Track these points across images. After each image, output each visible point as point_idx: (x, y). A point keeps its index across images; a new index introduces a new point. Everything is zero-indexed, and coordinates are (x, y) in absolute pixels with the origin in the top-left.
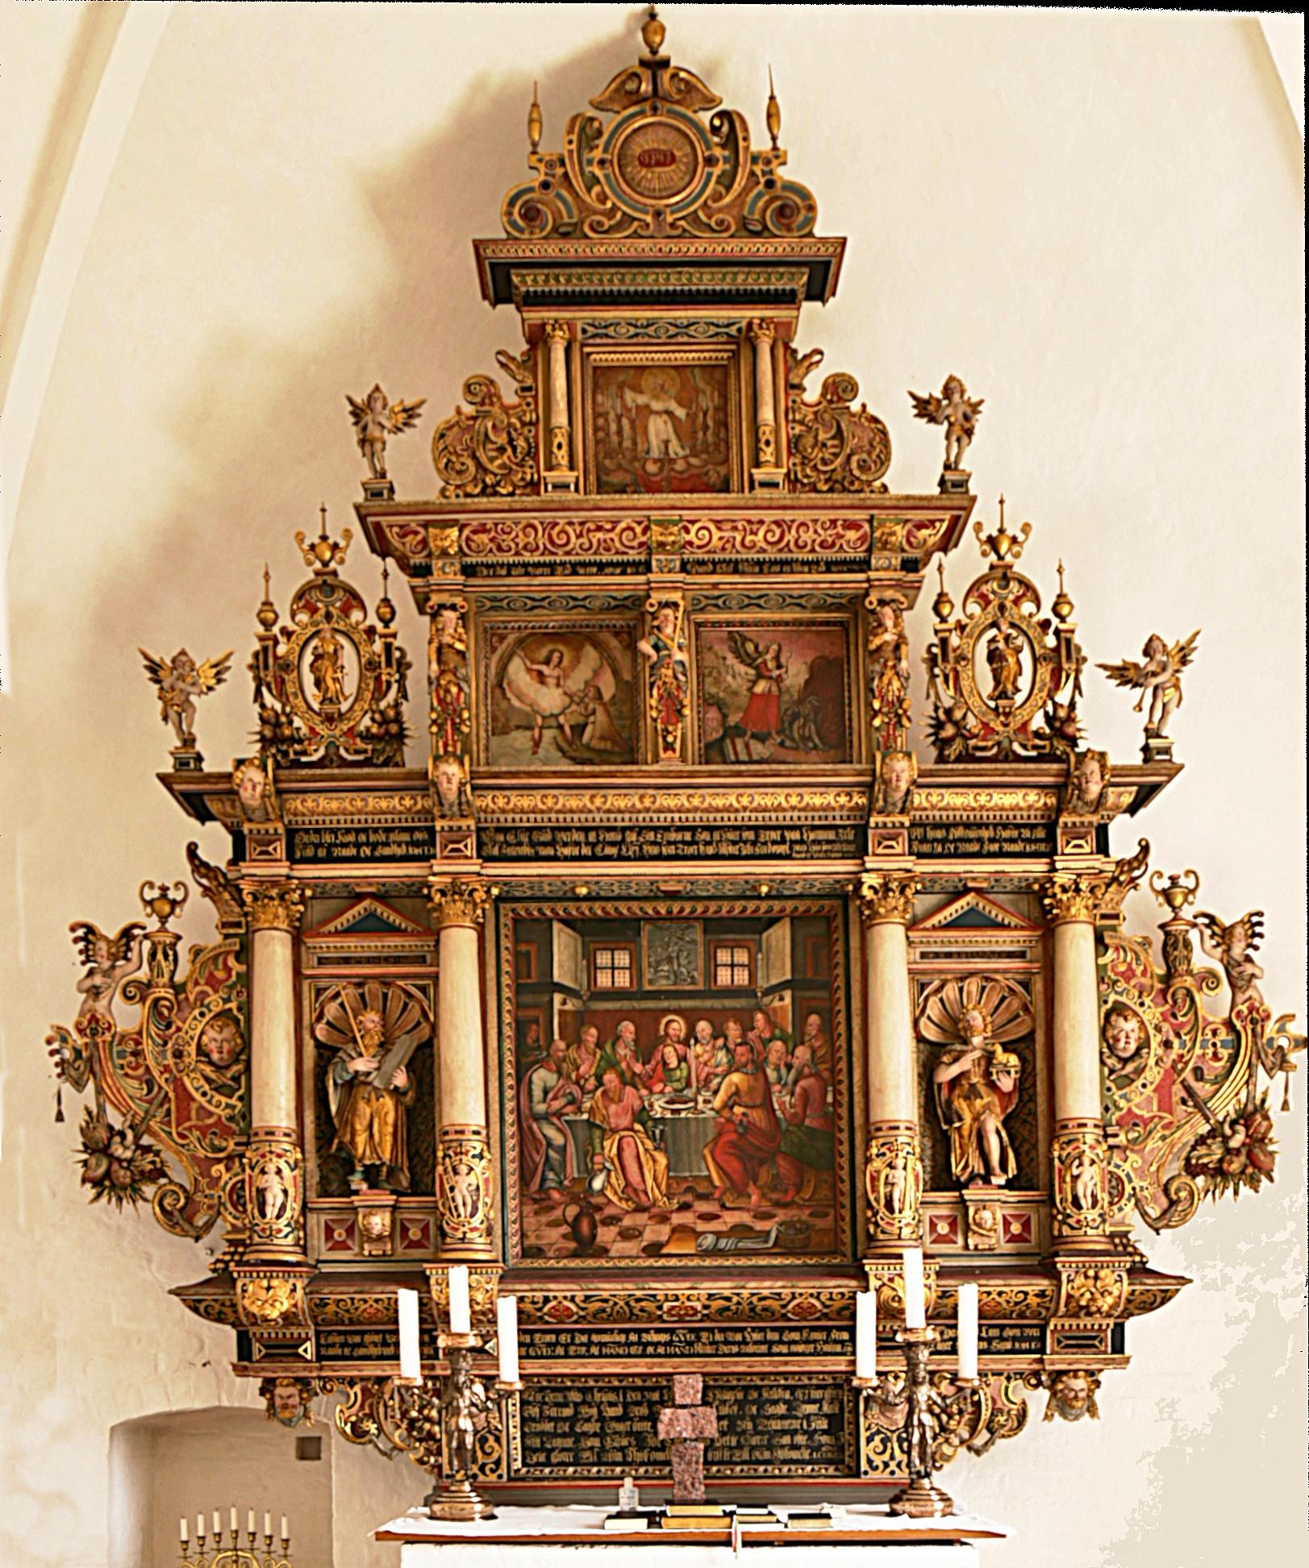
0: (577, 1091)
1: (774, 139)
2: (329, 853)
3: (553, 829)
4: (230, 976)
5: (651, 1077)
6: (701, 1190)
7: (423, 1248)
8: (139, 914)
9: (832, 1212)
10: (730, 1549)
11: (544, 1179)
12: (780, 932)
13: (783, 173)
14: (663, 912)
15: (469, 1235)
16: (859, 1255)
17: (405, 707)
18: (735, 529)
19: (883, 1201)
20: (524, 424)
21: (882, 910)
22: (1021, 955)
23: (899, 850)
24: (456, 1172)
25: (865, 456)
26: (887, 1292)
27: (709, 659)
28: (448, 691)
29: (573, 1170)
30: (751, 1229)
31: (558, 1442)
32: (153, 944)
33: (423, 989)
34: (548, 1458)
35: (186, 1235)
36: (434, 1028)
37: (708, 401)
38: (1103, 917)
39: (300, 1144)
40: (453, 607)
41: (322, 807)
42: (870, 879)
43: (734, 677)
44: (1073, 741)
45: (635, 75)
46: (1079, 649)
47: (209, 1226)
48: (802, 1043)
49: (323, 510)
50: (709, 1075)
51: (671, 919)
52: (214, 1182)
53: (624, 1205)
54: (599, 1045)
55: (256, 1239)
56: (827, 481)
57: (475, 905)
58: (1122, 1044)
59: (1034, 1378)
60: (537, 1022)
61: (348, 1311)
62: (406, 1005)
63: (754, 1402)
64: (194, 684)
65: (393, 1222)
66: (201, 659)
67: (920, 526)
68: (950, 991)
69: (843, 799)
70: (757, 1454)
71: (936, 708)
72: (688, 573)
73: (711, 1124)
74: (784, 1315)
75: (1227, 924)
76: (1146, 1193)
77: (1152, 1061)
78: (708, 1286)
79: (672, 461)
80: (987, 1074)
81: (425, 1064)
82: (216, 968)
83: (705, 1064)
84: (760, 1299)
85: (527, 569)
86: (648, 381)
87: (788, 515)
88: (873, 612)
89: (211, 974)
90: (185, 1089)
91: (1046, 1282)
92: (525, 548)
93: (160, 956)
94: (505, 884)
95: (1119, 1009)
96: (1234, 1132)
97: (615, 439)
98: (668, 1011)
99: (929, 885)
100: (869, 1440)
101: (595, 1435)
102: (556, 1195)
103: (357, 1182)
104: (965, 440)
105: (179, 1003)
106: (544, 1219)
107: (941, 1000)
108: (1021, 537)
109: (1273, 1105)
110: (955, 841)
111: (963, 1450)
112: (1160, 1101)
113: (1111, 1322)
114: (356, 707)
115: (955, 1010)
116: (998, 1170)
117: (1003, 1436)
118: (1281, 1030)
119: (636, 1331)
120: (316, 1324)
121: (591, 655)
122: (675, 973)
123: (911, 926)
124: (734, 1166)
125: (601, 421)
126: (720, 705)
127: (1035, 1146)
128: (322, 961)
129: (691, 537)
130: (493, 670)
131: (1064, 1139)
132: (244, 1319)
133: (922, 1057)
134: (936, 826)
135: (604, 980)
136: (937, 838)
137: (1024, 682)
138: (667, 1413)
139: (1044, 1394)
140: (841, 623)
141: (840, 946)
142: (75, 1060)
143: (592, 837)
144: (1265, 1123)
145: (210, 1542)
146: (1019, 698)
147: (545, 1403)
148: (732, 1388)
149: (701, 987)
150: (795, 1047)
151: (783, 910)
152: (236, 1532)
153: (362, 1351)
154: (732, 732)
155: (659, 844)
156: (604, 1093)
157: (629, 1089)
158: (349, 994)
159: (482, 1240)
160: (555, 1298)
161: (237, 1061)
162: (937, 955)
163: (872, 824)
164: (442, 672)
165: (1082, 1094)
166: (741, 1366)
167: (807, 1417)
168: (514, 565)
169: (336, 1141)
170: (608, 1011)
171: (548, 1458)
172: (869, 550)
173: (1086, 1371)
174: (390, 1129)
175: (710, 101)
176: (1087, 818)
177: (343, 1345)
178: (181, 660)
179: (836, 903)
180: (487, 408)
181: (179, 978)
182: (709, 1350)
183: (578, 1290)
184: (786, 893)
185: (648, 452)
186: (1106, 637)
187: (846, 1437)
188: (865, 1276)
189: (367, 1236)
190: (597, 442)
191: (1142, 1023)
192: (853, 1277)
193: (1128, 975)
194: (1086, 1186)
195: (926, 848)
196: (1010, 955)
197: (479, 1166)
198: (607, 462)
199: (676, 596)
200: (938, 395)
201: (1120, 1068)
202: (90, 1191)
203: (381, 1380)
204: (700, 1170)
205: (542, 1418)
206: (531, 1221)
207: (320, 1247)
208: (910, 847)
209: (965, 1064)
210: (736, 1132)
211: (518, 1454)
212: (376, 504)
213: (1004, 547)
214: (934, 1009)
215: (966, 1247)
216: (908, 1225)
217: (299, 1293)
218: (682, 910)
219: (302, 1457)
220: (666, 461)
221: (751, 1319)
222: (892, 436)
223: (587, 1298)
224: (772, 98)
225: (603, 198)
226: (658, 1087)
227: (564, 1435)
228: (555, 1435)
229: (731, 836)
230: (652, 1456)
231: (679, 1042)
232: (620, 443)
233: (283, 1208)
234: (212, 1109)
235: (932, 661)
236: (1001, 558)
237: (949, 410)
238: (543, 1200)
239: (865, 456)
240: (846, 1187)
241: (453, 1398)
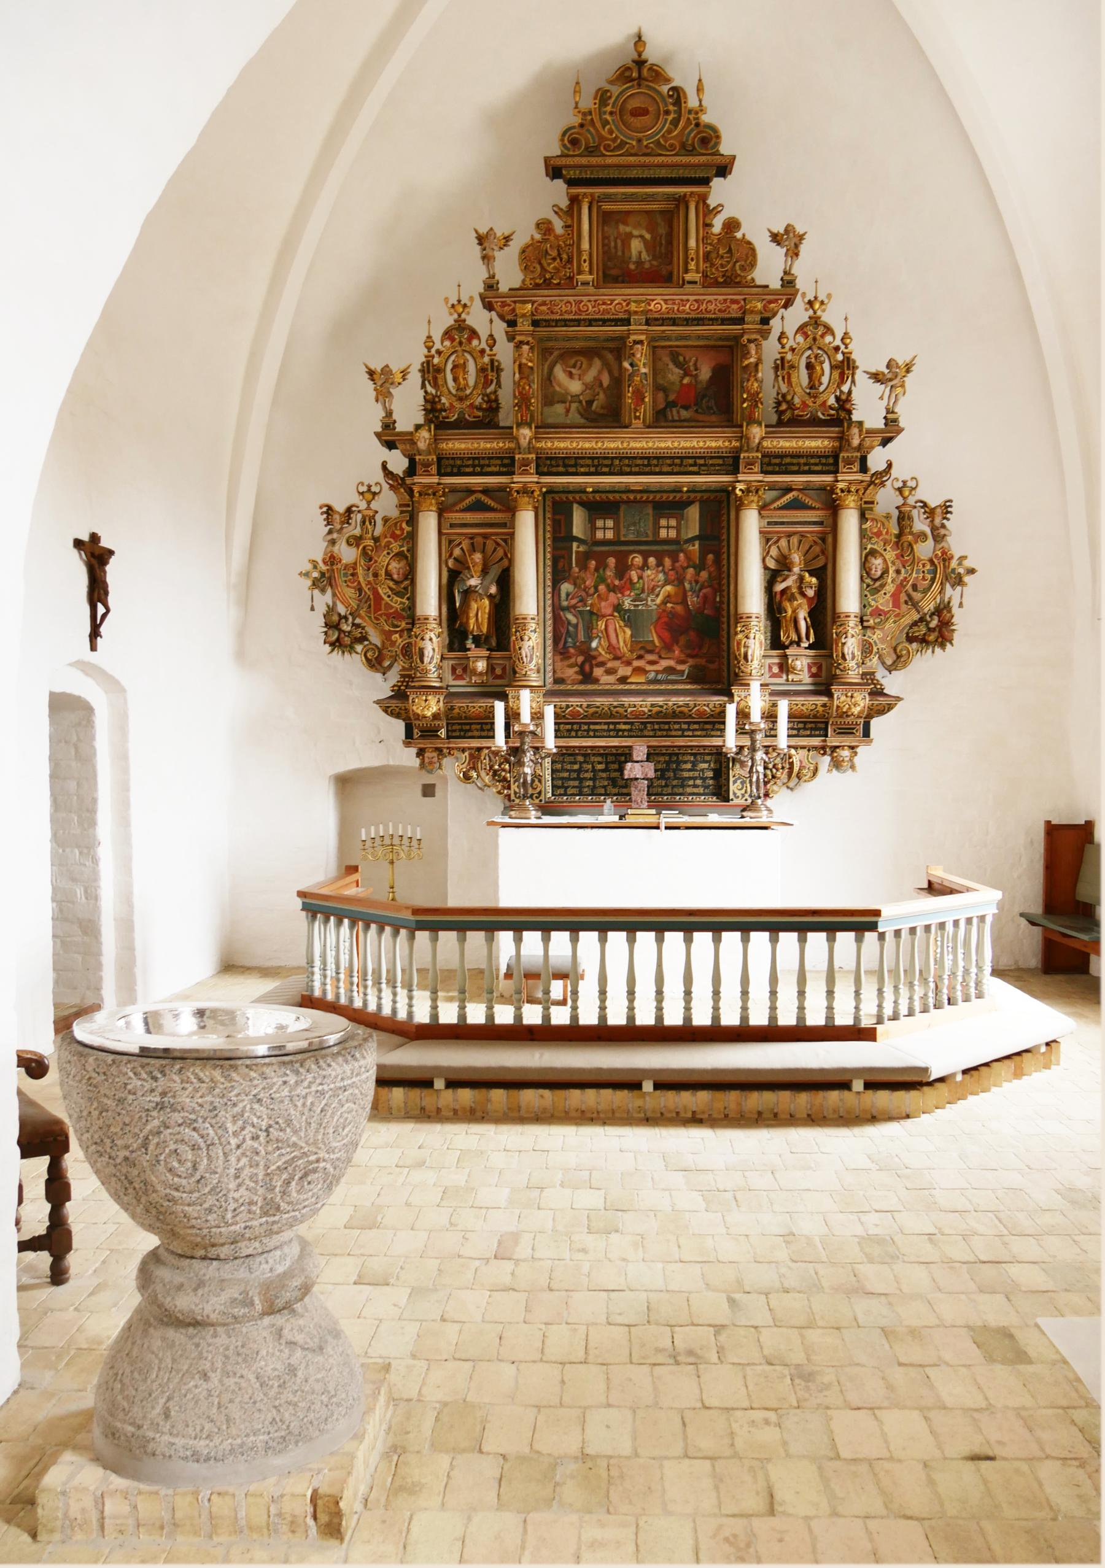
0: (583, 594)
1: (700, 101)
2: (459, 470)
3: (576, 458)
7: (503, 681)
8: (355, 499)
13: (705, 118)
17: (500, 392)
20: (566, 245)
22: (821, 523)
23: (756, 470)
24: (522, 640)
26: (743, 704)
28: (524, 388)
29: (581, 637)
31: (571, 783)
33: (505, 541)
35: (377, 671)
37: (662, 230)
38: (866, 503)
39: (440, 624)
40: (527, 343)
41: (458, 445)
44: (849, 412)
47: (390, 666)
52: (393, 643)
53: (608, 656)
54: (597, 569)
59: (822, 749)
66: (395, 368)
67: (770, 302)
68: (783, 543)
69: (727, 444)
71: (778, 394)
75: (933, 506)
77: (889, 580)
78: (651, 700)
80: (800, 588)
81: (506, 582)
86: (632, 219)
91: (826, 699)
97: (613, 250)
99: (772, 487)
100: (735, 782)
101: (590, 779)
102: (572, 650)
103: (470, 644)
106: (566, 663)
108: (826, 301)
109: (955, 604)
111: (784, 788)
113: (862, 720)
115: (785, 551)
118: (960, 564)
119: (613, 723)
121: (597, 363)
123: (762, 508)
124: (666, 635)
126: (665, 390)
128: (452, 526)
129: (652, 307)
130: (546, 371)
133: (768, 577)
135: (599, 535)
136: (774, 463)
137: (825, 380)
140: (729, 347)
145: (378, 841)
146: (822, 388)
148: (663, 754)
149: (650, 538)
153: (470, 734)
154: (671, 405)
161: (406, 579)
162: (776, 523)
164: (521, 378)
167: (702, 770)
168: (560, 320)
172: (744, 313)
175: (668, 80)
176: (855, 454)
177: (460, 730)
181: (377, 533)
182: (651, 733)
186: (868, 357)
189: (474, 672)
191: (885, 560)
193: (878, 534)
195: (770, 468)
197: (534, 636)
199: (643, 337)
201: (870, 582)
202: (327, 648)
205: (563, 770)
206: (559, 664)
207: (449, 680)
213: (817, 306)
215: (787, 680)
217: (441, 704)
219: (433, 795)
220: (640, 263)
221: (673, 717)
223: (588, 706)
224: (700, 80)
225: (611, 132)
226: (628, 593)
227: (574, 779)
228: (569, 779)
229: (668, 461)
230: (619, 788)
233: (432, 658)
235: (776, 368)
237: (789, 240)
240: (725, 647)
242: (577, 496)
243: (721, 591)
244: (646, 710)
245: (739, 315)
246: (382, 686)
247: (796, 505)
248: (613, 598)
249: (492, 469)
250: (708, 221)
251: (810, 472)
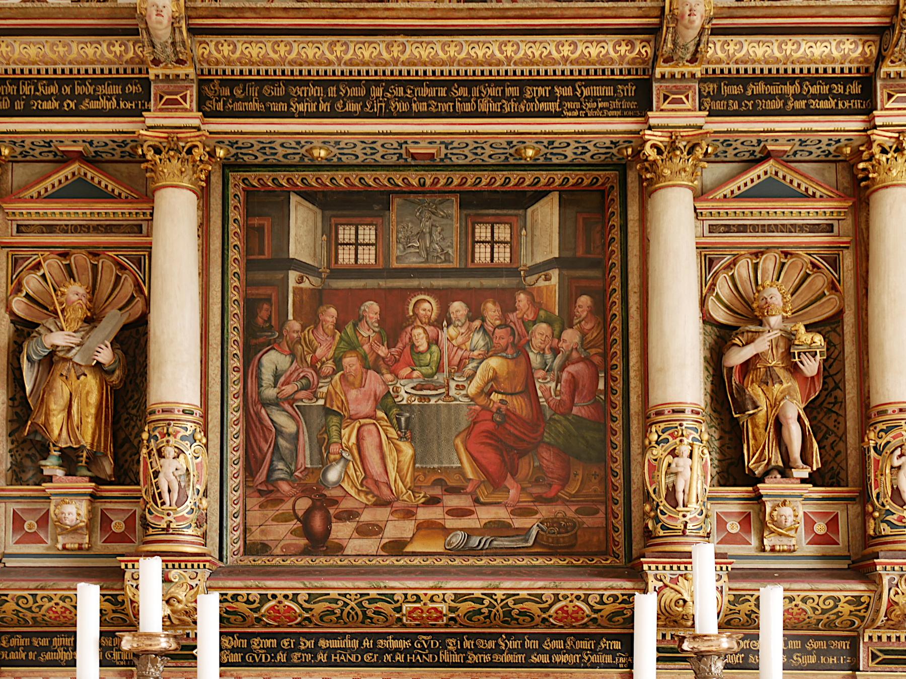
0: (310, 374)
3: (287, 83)
5: (397, 361)
6: (451, 483)
9: (603, 508)
11: (271, 470)
12: (547, 209)
14: (415, 182)
15: (173, 525)
16: (635, 554)
19: (664, 492)
21: (667, 172)
22: (829, 228)
23: (688, 105)
24: (161, 455)
26: (669, 595)
29: (305, 459)
30: (508, 526)
33: (138, 262)
36: (147, 302)
42: (655, 137)
50: (465, 360)
51: (423, 193)
53: (363, 498)
60: (268, 300)
61: (30, 609)
62: (118, 278)
68: (743, 270)
73: (465, 410)
74: (544, 620)
81: (134, 341)
83: (459, 347)
91: (862, 587)
94: (231, 144)
102: (285, 487)
103: (52, 466)
106: (271, 513)
110: (754, 97)
115: (747, 289)
123: (700, 195)
124: (490, 457)
127: (843, 438)
131: (880, 426)
133: (710, 340)
134: (731, 81)
135: (346, 257)
136: (734, 92)
141: (616, 221)
149: (455, 264)
153: (49, 656)
155: (410, 101)
160: (274, 596)
162: (728, 229)
163: (658, 76)
169: (29, 422)
179: (612, 174)
184: (555, 160)
192: (629, 578)
195: (719, 105)
196: (814, 229)
204: (451, 461)
206: (255, 516)
209: (761, 345)
210: (492, 420)
214: (723, 288)
218: (436, 181)
223: (311, 598)
226: (406, 371)
229: (492, 91)
231: (429, 324)
238: (271, 491)
240: (619, 481)
242: (297, 177)
243: (608, 369)
244: (444, 608)
247: (769, 190)
248: (374, 383)
249: (103, 103)
251: (808, 112)
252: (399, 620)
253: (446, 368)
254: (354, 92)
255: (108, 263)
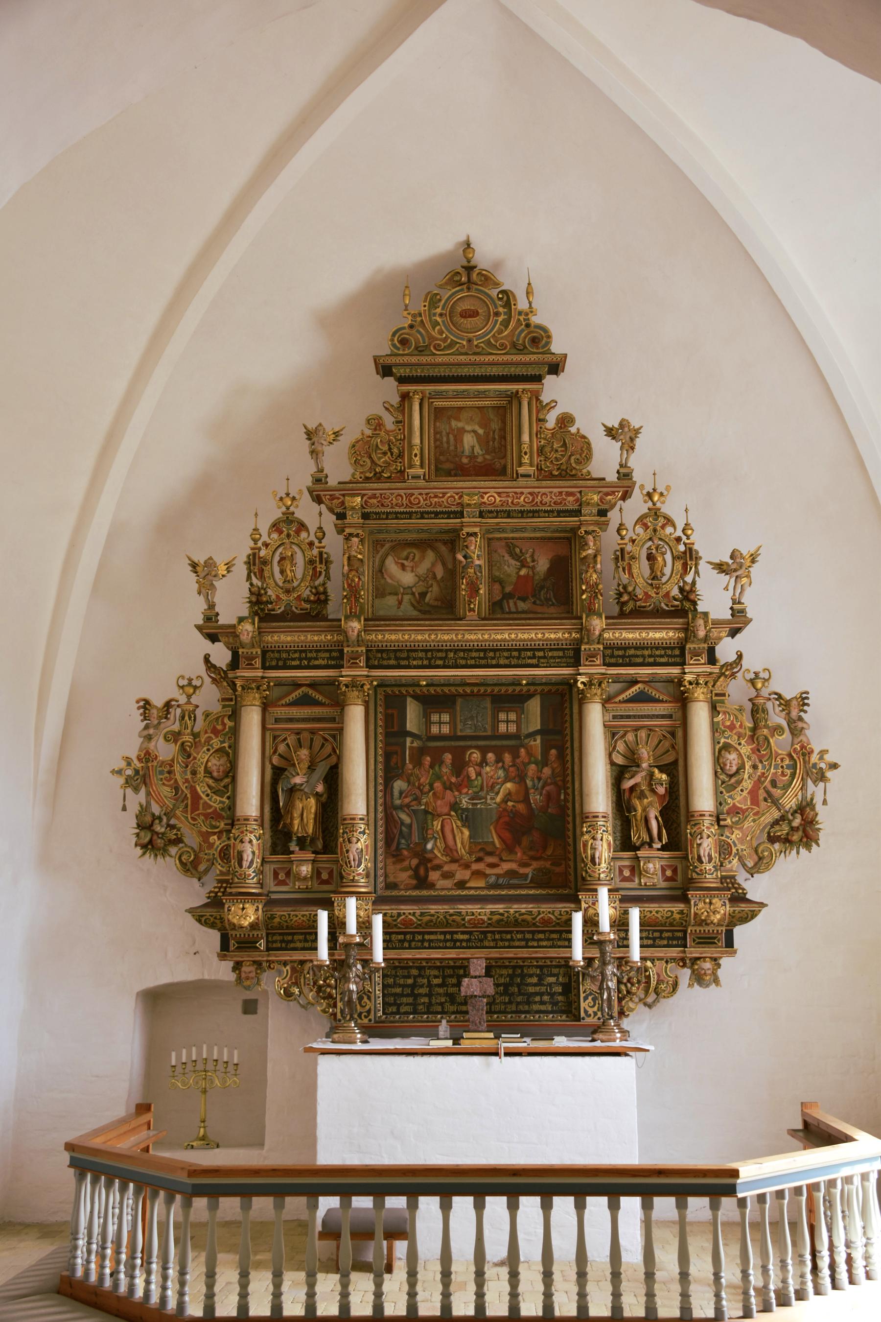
0: (418, 792)
2: (285, 663)
3: (408, 651)
4: (225, 728)
5: (460, 785)
10: (498, 1058)
11: (399, 843)
13: (535, 320)
17: (329, 585)
18: (508, 496)
22: (670, 717)
23: (598, 662)
24: (350, 842)
25: (578, 456)
26: (591, 911)
27: (495, 557)
28: (353, 580)
29: (415, 838)
31: (404, 1000)
32: (182, 710)
33: (334, 737)
34: (398, 1009)
35: (193, 876)
37: (495, 425)
38: (716, 695)
39: (262, 825)
40: (357, 535)
41: (283, 638)
43: (508, 566)
45: (458, 273)
46: (697, 552)
47: (207, 871)
48: (547, 765)
49: (288, 479)
50: (495, 785)
52: (211, 846)
53: (444, 859)
54: (432, 766)
55: (236, 880)
56: (558, 469)
57: (364, 692)
58: (728, 767)
59: (683, 962)
62: (323, 744)
63: (518, 976)
64: (215, 576)
65: (313, 869)
67: (607, 494)
68: (630, 737)
69: (566, 635)
70: (521, 1007)
72: (483, 518)
76: (745, 853)
77: (746, 776)
78: (491, 907)
79: (476, 457)
80: (650, 785)
81: (334, 780)
82: (218, 724)
83: (491, 777)
84: (520, 915)
85: (397, 516)
86: (464, 415)
87: (536, 490)
88: (582, 537)
89: (214, 727)
90: (197, 792)
91: (682, 905)
92: (396, 505)
93: (187, 718)
95: (727, 747)
96: (794, 818)
97: (445, 445)
98: (470, 747)
99: (617, 679)
100: (586, 998)
101: (426, 995)
102: (405, 853)
103: (293, 846)
104: (631, 451)
105: (195, 743)
106: (398, 866)
107: (625, 742)
108: (665, 493)
110: (629, 656)
111: (641, 1006)
112: (751, 799)
113: (724, 929)
114: (302, 584)
115: (632, 745)
116: (657, 840)
117: (664, 997)
119: (450, 933)
120: (267, 929)
122: (475, 725)
124: (507, 835)
125: (438, 436)
126: (501, 582)
128: (277, 721)
129: (485, 500)
131: (693, 823)
132: (227, 926)
133: (614, 774)
134: (619, 649)
135: (435, 730)
136: (618, 655)
137: (668, 570)
138: (466, 981)
139: (687, 972)
140: (567, 538)
142: (135, 776)
143: (429, 655)
144: (812, 813)
145: (190, 1067)
146: (664, 579)
147: (398, 976)
149: (489, 733)
150: (542, 768)
151: (536, 690)
152: (206, 1059)
153: (292, 945)
154: (507, 596)
155: (466, 659)
156: (434, 793)
157: (448, 792)
158: (291, 740)
159: (363, 880)
160: (404, 914)
161: (227, 776)
162: (622, 717)
165: (704, 798)
166: (510, 953)
167: (550, 985)
170: (436, 747)
171: (398, 1009)
173: (711, 958)
174: (313, 816)
175: (497, 284)
178: (210, 563)
180: (377, 432)
181: (196, 730)
183: (416, 909)
185: (463, 452)
186: (711, 548)
187: (572, 997)
188: (578, 902)
189: (298, 877)
190: (436, 447)
191: (740, 755)
193: (732, 727)
194: (704, 851)
196: (663, 717)
198: (441, 457)
199: (477, 530)
200: (616, 426)
202: (139, 851)
203: (302, 962)
205: (395, 985)
206: (391, 868)
208: (604, 660)
209: (638, 779)
211: (380, 1007)
212: (318, 487)
213: (656, 498)
216: (603, 872)
218: (479, 691)
220: (472, 457)
222: (593, 446)
223: (422, 914)
224: (529, 284)
225: (441, 332)
226: (465, 790)
227: (407, 995)
229: (506, 654)
231: (477, 765)
232: (448, 448)
233: (252, 862)
234: (212, 804)
236: (654, 504)
237: (624, 434)
239: (578, 456)
240: (571, 849)
241: (346, 972)
242: (411, 690)
244: (485, 918)
245: (576, 507)
246: (196, 893)
247: (642, 698)
248: (449, 796)
250: (541, 417)
252: (464, 924)
253: (485, 788)
254: (440, 655)
255: (319, 737)
